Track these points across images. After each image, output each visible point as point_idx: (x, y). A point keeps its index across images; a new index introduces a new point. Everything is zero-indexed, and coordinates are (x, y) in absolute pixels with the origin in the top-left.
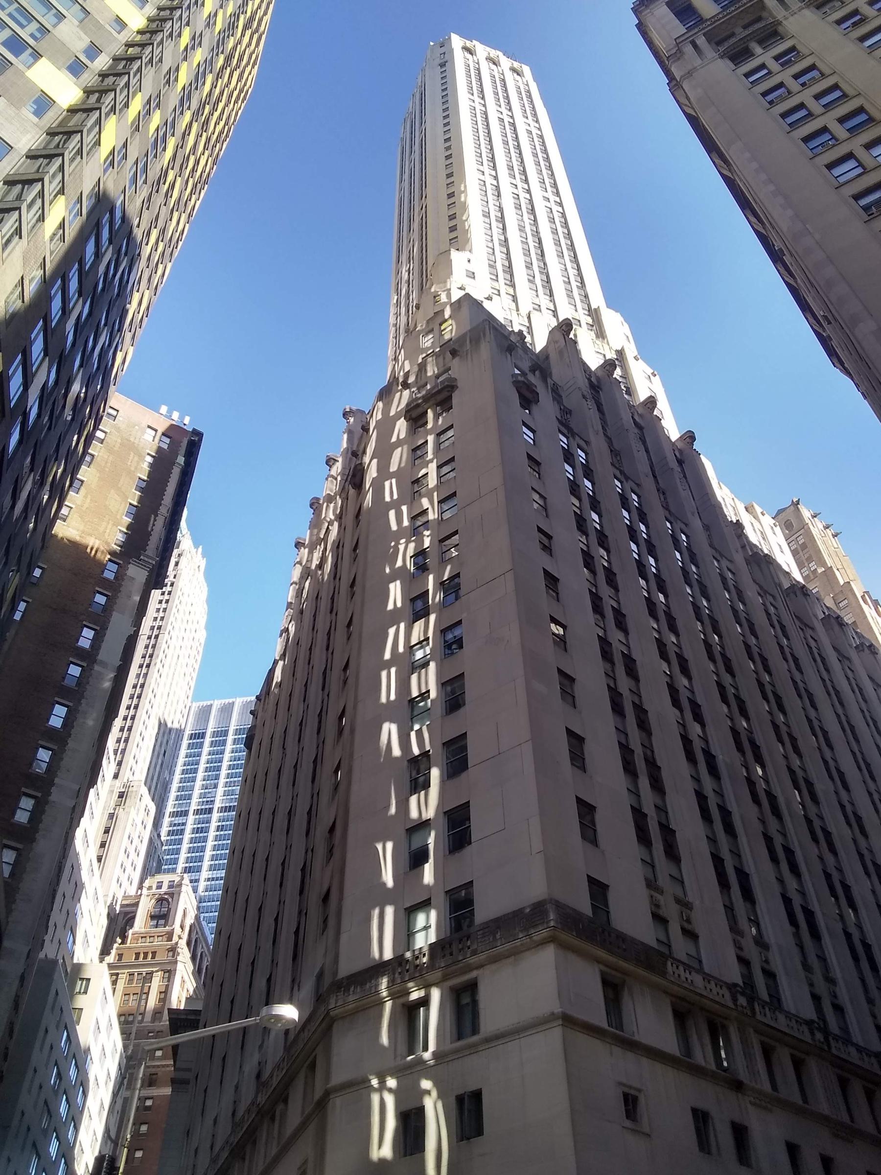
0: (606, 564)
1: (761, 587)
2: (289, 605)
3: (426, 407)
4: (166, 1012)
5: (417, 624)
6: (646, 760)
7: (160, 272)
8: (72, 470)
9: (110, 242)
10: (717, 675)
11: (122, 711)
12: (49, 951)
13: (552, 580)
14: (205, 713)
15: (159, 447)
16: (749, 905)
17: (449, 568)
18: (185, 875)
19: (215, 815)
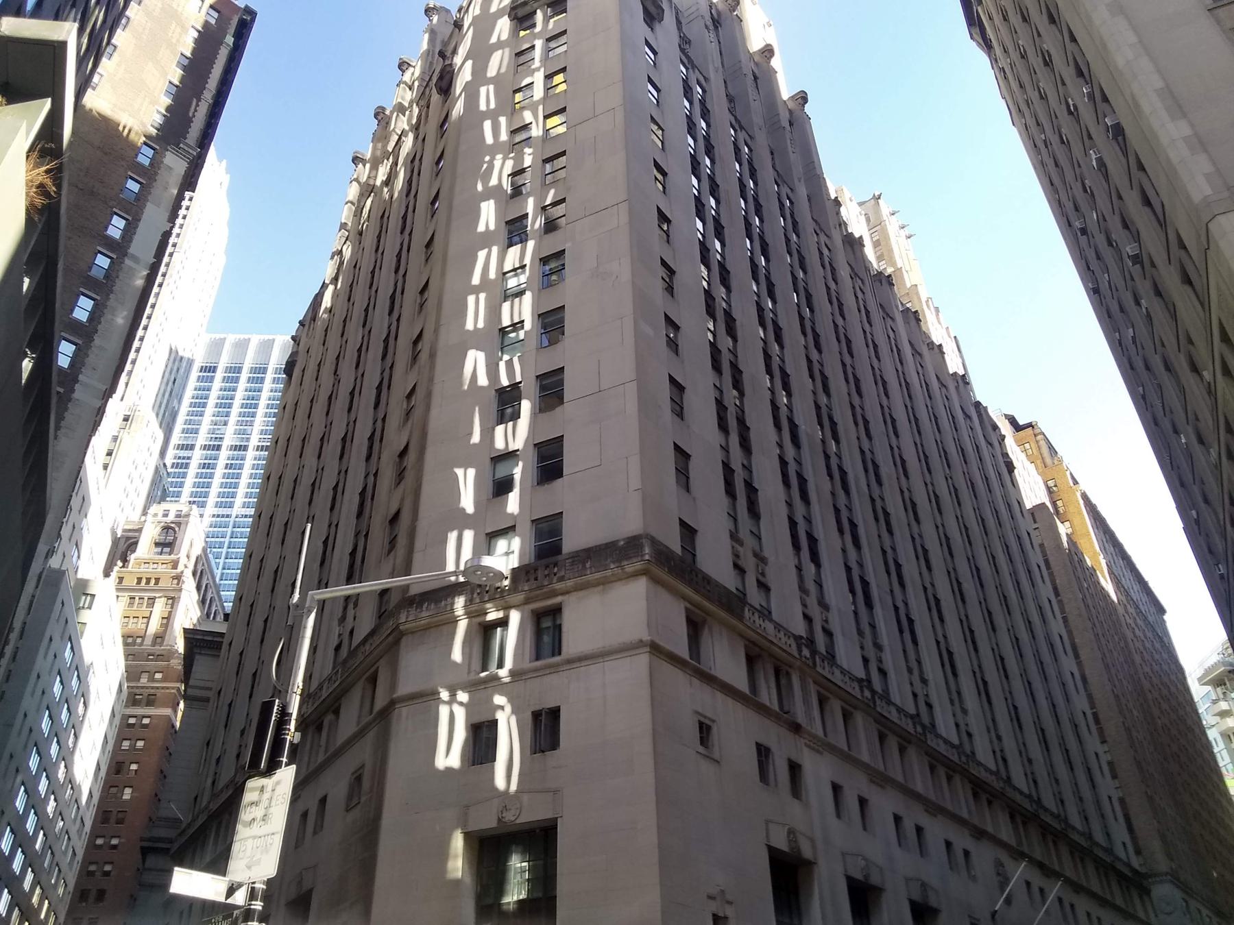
2: (343, 226)
3: (535, 5)
14: (217, 346)
17: (552, 192)
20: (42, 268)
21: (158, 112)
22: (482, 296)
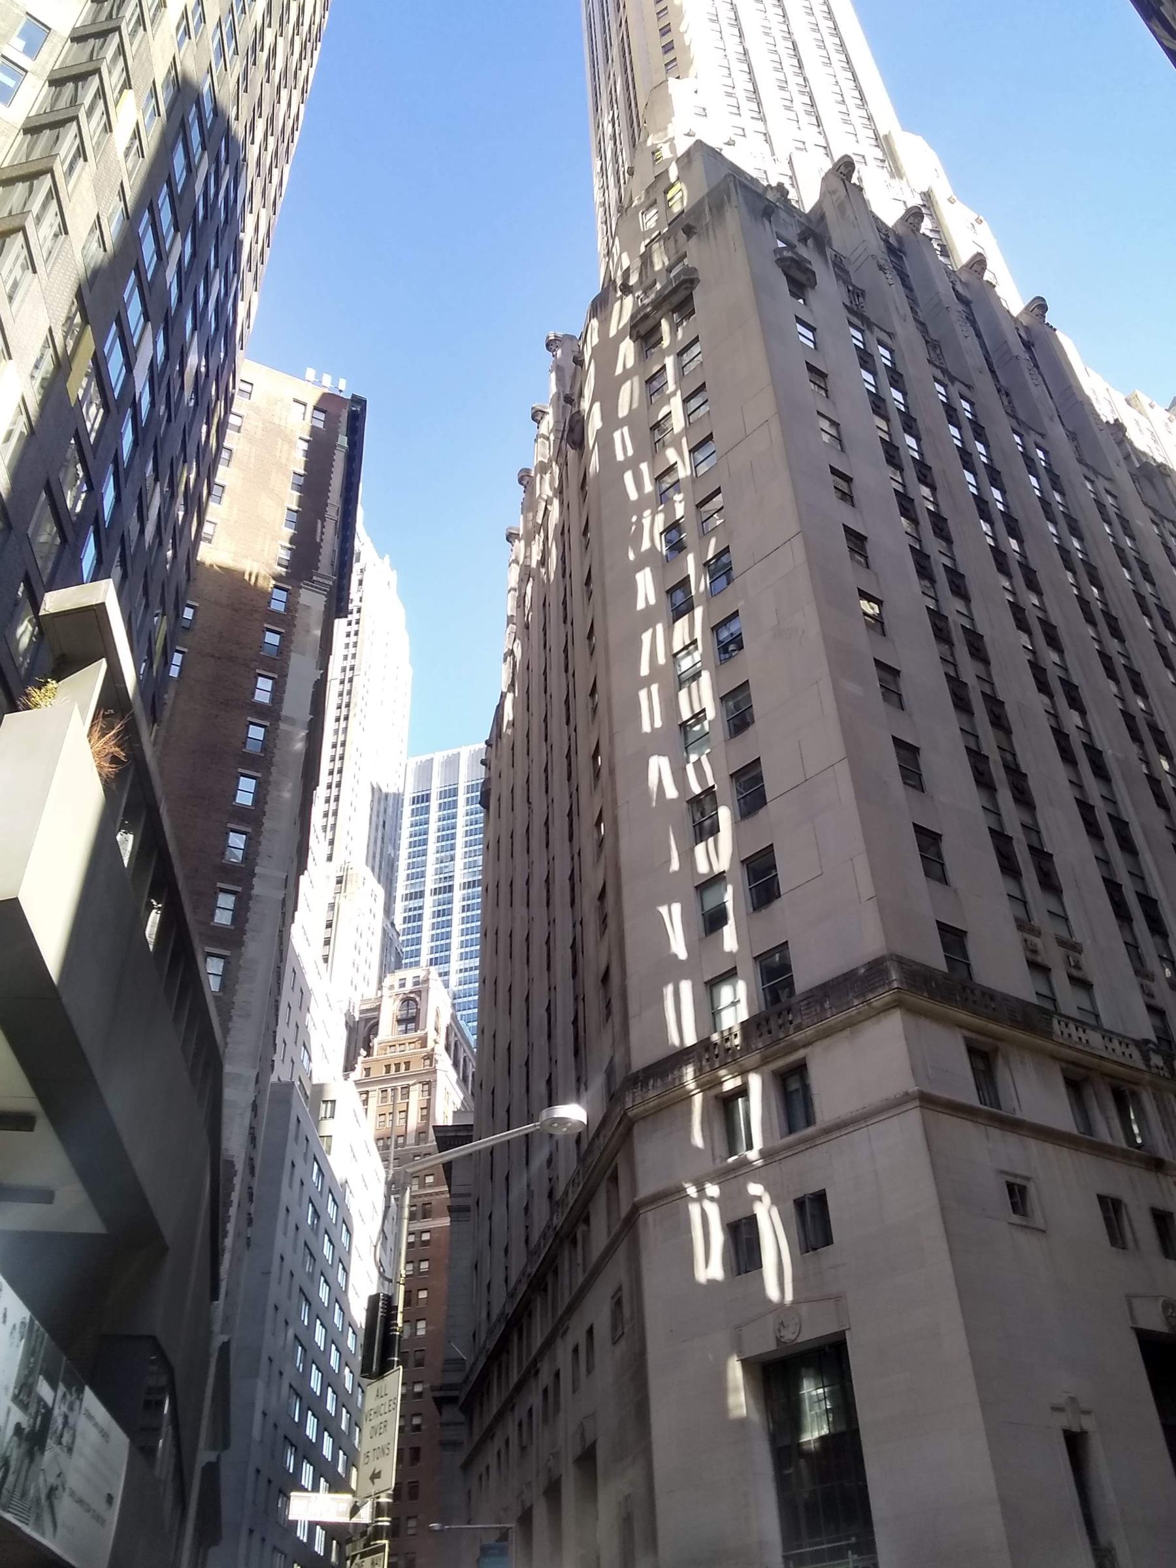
0: (931, 508)
1: (1155, 511)
2: (510, 620)
4: (431, 1131)
5: (679, 624)
6: (1006, 766)
7: (275, 180)
8: (208, 472)
9: (204, 149)
10: (1099, 642)
11: (324, 778)
12: (281, 1073)
13: (856, 541)
14: (425, 770)
15: (313, 427)
16: (1158, 940)
17: (713, 541)
18: (432, 969)
19: (458, 894)
20: (143, 820)
21: (283, 547)
22: (655, 688)
